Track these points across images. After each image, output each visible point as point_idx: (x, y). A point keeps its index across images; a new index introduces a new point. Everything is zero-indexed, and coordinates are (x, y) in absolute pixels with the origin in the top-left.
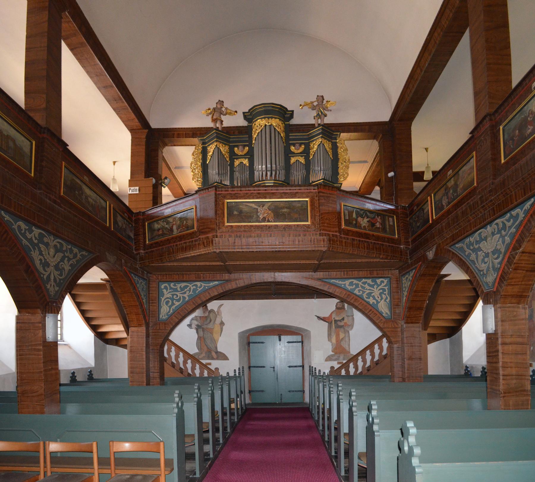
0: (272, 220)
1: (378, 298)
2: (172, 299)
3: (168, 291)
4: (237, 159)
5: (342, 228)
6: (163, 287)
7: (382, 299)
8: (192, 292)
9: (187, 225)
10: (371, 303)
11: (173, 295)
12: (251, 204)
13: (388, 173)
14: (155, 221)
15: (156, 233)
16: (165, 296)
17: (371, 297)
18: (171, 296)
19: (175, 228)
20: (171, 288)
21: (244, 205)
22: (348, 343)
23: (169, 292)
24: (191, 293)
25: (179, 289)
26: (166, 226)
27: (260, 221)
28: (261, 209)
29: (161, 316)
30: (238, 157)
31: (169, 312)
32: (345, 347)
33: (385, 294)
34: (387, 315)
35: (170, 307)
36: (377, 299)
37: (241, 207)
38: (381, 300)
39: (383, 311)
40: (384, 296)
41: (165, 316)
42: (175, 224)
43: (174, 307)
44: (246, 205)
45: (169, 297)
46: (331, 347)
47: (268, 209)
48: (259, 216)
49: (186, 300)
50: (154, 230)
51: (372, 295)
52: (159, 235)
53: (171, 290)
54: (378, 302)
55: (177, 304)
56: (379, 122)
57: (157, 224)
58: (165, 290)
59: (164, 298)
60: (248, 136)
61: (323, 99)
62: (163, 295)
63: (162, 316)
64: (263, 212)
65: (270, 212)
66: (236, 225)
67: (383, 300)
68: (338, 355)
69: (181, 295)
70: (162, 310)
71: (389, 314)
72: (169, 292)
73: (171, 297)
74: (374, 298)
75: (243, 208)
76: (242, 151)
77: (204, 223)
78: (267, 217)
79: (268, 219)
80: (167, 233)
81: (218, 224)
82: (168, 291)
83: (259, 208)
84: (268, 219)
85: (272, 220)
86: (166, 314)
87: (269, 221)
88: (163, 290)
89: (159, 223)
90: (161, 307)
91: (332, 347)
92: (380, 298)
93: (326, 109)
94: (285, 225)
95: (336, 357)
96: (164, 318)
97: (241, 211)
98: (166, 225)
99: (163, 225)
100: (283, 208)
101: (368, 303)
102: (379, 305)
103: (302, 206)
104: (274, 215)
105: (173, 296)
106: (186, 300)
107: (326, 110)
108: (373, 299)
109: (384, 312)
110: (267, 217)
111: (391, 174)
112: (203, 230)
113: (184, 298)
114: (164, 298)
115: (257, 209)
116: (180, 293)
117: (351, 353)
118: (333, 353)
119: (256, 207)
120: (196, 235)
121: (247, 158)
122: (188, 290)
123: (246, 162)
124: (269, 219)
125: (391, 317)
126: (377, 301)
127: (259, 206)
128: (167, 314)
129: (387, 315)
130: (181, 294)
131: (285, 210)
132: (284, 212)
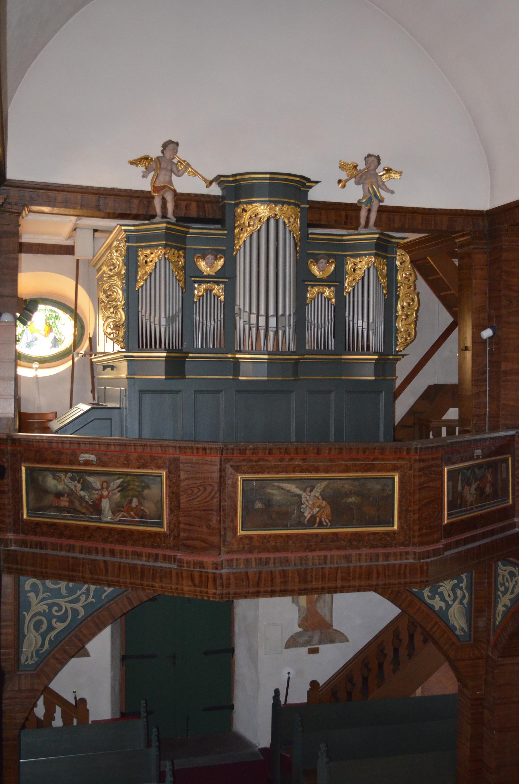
0: (327, 521)
1: (449, 596)
2: (49, 616)
3: (41, 596)
4: (200, 283)
5: (444, 524)
6: (27, 587)
7: (455, 598)
8: (93, 598)
9: (143, 510)
10: (437, 608)
11: (50, 606)
12: (289, 485)
13: (481, 332)
14: (47, 470)
15: (49, 500)
16: (34, 609)
17: (437, 596)
18: (46, 608)
19: (106, 505)
20: (47, 589)
21: (274, 486)
22: (330, 603)
23: (43, 599)
24: (90, 600)
25: (64, 592)
26: (82, 493)
27: (304, 524)
28: (308, 498)
29: (23, 659)
30: (202, 278)
31: (42, 646)
32: (323, 614)
33: (461, 589)
34: (462, 633)
35: (44, 636)
36: (447, 599)
37: (269, 491)
38: (454, 601)
39: (456, 625)
40: (459, 592)
41: (32, 657)
42: (107, 496)
43: (52, 634)
44: (280, 488)
45: (39, 610)
46: (297, 616)
47: (320, 497)
48: (304, 513)
49: (80, 617)
50: (46, 492)
51: (439, 590)
52: (60, 509)
53: (45, 595)
54: (448, 606)
55: (60, 626)
56: (467, 211)
57: (54, 478)
58: (32, 595)
59: (31, 613)
60: (226, 232)
61: (379, 163)
62: (29, 605)
63: (25, 657)
64: (311, 502)
65: (324, 503)
66: (258, 535)
67: (457, 602)
68: (310, 633)
69: (69, 606)
70: (26, 644)
71: (467, 631)
72: (43, 599)
73: (47, 611)
74: (443, 599)
75: (273, 495)
76: (211, 266)
77: (190, 525)
78: (319, 514)
79: (320, 519)
80: (84, 511)
81: (222, 532)
82: (41, 596)
83: (304, 495)
84: (320, 519)
85: (327, 521)
86: (34, 654)
87: (321, 525)
88: (29, 594)
89: (60, 478)
90: (25, 636)
91: (299, 617)
92: (452, 597)
93: (383, 187)
94: (352, 534)
95: (306, 638)
96: (30, 662)
97: (269, 501)
98: (81, 490)
99: (73, 487)
100: (348, 495)
101: (431, 608)
102: (451, 611)
103: (383, 490)
104: (332, 512)
105: (50, 609)
106: (80, 617)
107: (383, 189)
108: (440, 600)
109: (458, 627)
110: (319, 514)
111: (487, 333)
112: (189, 542)
113: (75, 612)
114: (31, 613)
115: (300, 496)
116: (66, 599)
117: (335, 627)
118: (300, 630)
119: (298, 491)
120: (165, 542)
121: (223, 282)
122: (83, 593)
123: (218, 290)
124: (323, 519)
125: (470, 637)
126: (446, 602)
127: (305, 491)
128: (37, 652)
129: (462, 633)
130: (69, 602)
131: (353, 499)
132: (351, 503)
